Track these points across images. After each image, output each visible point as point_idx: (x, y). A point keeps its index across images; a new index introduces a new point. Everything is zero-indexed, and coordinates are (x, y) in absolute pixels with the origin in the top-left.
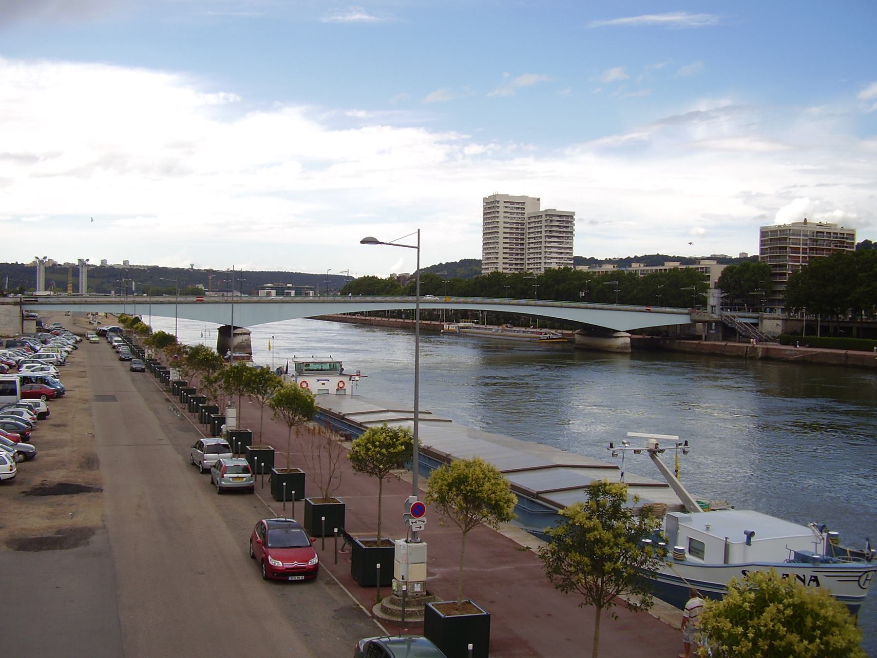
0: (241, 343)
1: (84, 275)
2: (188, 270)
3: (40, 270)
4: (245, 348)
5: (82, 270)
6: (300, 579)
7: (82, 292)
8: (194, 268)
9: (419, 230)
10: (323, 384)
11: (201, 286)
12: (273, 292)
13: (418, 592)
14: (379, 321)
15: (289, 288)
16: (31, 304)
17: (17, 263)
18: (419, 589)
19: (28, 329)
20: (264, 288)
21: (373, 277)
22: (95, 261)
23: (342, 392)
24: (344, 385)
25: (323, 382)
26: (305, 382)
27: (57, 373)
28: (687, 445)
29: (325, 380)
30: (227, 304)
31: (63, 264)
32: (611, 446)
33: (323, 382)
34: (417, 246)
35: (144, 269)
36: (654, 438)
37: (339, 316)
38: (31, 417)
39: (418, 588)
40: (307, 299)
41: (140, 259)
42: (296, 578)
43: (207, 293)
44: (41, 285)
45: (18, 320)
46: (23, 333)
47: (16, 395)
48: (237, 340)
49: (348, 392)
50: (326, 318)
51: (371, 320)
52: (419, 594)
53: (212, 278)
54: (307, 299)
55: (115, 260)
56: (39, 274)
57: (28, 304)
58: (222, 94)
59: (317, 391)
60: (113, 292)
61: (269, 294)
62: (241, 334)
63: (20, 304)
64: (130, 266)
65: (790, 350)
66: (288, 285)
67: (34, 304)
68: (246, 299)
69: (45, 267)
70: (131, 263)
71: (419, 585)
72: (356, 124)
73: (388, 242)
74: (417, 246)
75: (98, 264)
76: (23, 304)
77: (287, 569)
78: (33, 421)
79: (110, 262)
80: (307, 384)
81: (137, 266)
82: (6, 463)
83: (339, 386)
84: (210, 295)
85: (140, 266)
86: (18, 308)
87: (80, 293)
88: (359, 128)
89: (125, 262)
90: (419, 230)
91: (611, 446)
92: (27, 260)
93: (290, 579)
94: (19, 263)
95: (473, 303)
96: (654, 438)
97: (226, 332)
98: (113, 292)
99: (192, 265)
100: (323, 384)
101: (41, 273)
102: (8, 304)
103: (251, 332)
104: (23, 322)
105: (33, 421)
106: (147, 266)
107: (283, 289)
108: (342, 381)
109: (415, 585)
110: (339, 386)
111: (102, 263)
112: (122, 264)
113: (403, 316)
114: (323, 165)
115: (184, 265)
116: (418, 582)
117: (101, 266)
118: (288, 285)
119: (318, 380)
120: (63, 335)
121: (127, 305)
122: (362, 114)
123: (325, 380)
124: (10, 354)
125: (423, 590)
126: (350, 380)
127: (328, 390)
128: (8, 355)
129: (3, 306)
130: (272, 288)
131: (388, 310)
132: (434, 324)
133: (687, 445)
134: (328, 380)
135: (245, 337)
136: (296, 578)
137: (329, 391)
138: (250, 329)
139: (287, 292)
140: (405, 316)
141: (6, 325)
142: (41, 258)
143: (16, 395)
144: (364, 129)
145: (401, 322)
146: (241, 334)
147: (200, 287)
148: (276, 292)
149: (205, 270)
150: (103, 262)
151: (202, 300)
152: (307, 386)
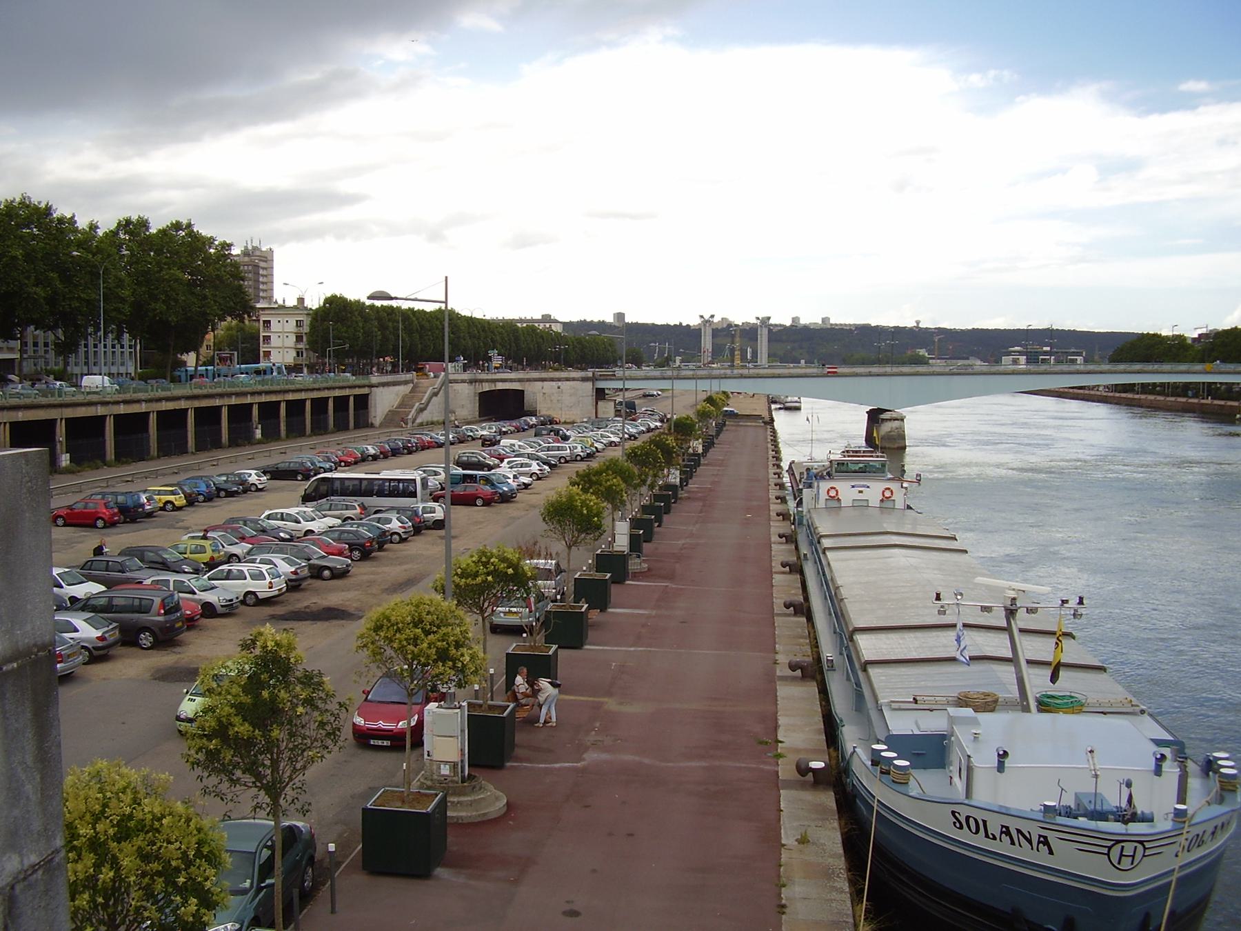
0: (890, 432)
1: (763, 339)
2: (911, 329)
3: (705, 332)
4: (895, 439)
5: (761, 331)
6: (385, 744)
7: (761, 362)
8: (921, 326)
9: (446, 278)
10: (861, 492)
11: (923, 352)
12: (1023, 359)
13: (447, 776)
14: (1151, 400)
15: (1046, 353)
16: (606, 380)
17: (681, 324)
18: (447, 772)
19: (604, 413)
20: (1009, 354)
21: (1155, 335)
22: (782, 318)
23: (888, 504)
24: (892, 494)
25: (861, 489)
26: (834, 488)
27: (541, 470)
28: (1083, 604)
29: (863, 486)
30: (871, 378)
31: (741, 324)
32: (938, 597)
33: (861, 489)
34: (444, 300)
35: (850, 329)
36: (1014, 590)
37: (1066, 390)
38: (401, 525)
39: (445, 770)
40: (1073, 368)
41: (846, 315)
42: (380, 743)
43: (931, 361)
44: (763, 352)
45: (589, 400)
46: (596, 417)
47: (416, 497)
48: (886, 428)
49: (899, 504)
50: (1080, 397)
51: (1140, 399)
52: (449, 779)
53: (939, 340)
54: (1073, 368)
55: (810, 317)
56: (705, 338)
57: (603, 380)
58: (992, 73)
59: (851, 501)
60: (803, 361)
61: (1015, 362)
62: (890, 420)
63: (593, 379)
64: (832, 325)
65: (364, 459)
66: (1045, 349)
67: (611, 380)
68: (985, 369)
69: (713, 329)
70: (832, 321)
71: (448, 767)
72: (1189, 103)
73: (404, 297)
74: (444, 300)
75: (788, 323)
76: (597, 380)
77: (368, 729)
78: (403, 530)
79: (805, 320)
80: (837, 491)
81: (841, 325)
82: (265, 579)
83: (883, 495)
84: (938, 364)
85: (846, 325)
86: (589, 385)
87: (759, 363)
88: (1194, 108)
89: (825, 320)
90: (446, 278)
91: (938, 597)
92: (694, 321)
93: (372, 743)
94: (684, 324)
95: (1188, 372)
96: (1014, 590)
97: (875, 417)
98: (803, 361)
99: (918, 322)
100: (861, 492)
101: (707, 338)
102: (574, 379)
103: (905, 417)
104: (597, 403)
105: (403, 530)
106: (855, 325)
107: (1038, 353)
108: (888, 489)
109: (442, 766)
110: (883, 495)
111: (793, 321)
112: (820, 322)
113: (1190, 393)
114: (1130, 166)
115: (909, 323)
116: (447, 762)
117: (792, 326)
118: (1045, 349)
119: (853, 487)
120: (639, 421)
121: (678, 381)
122: (1200, 86)
123: (863, 486)
124: (519, 446)
125: (452, 774)
126: (902, 487)
127: (867, 500)
128: (516, 448)
129: (568, 382)
130: (1021, 353)
131: (1204, 383)
132: (1231, 406)
133: (1083, 604)
134: (868, 487)
135: (896, 424)
136: (380, 743)
137: (870, 502)
138: (903, 411)
139: (1042, 359)
140: (1193, 394)
141: (571, 407)
142: (707, 317)
143: (416, 497)
144: (1201, 109)
145: (1183, 402)
146: (890, 420)
147: (921, 354)
148: (1027, 359)
149: (935, 328)
150: (795, 320)
151: (836, 372)
152: (837, 494)
